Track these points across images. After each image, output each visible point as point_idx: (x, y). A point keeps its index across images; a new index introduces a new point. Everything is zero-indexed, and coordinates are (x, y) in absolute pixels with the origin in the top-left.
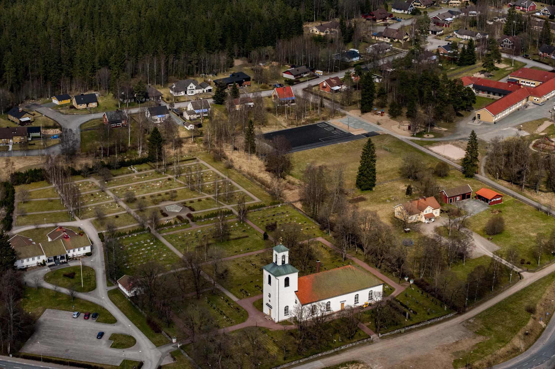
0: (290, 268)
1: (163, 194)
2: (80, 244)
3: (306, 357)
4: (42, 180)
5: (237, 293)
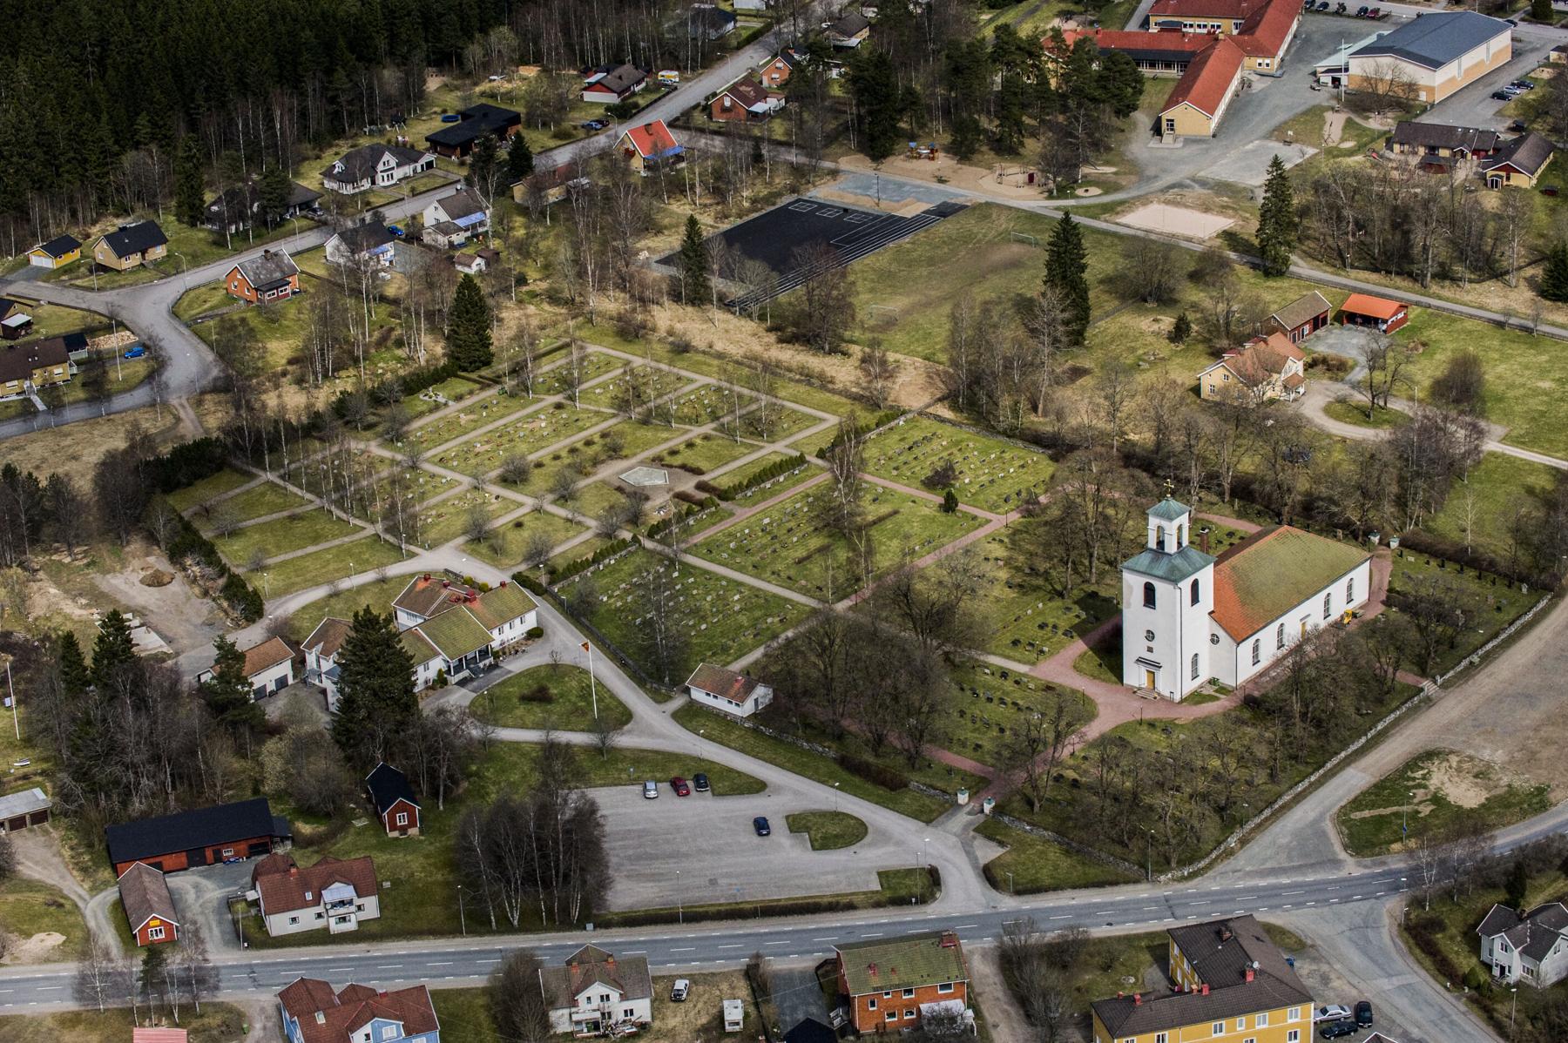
0: (1195, 554)
1: (579, 445)
2: (512, 610)
3: (1317, 769)
4: (220, 468)
5: (1007, 652)
